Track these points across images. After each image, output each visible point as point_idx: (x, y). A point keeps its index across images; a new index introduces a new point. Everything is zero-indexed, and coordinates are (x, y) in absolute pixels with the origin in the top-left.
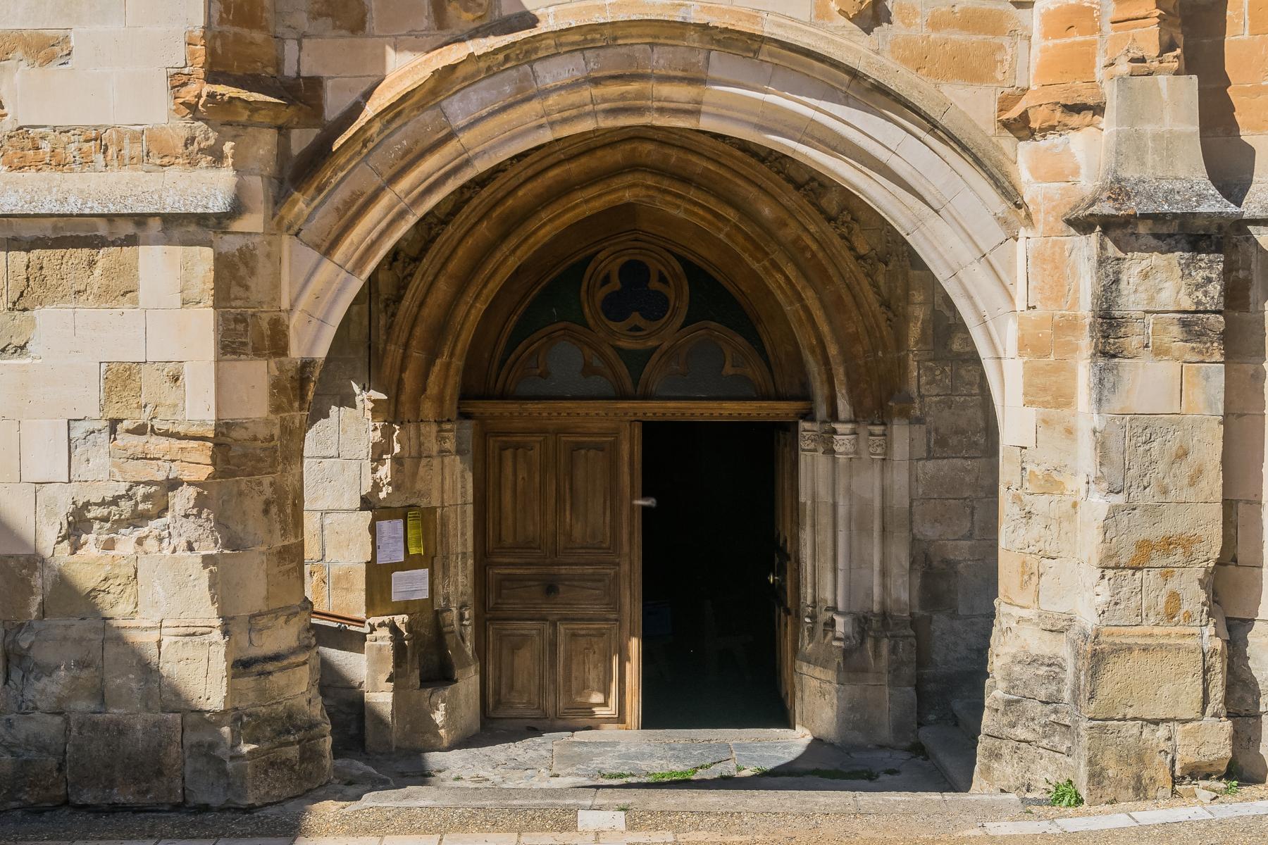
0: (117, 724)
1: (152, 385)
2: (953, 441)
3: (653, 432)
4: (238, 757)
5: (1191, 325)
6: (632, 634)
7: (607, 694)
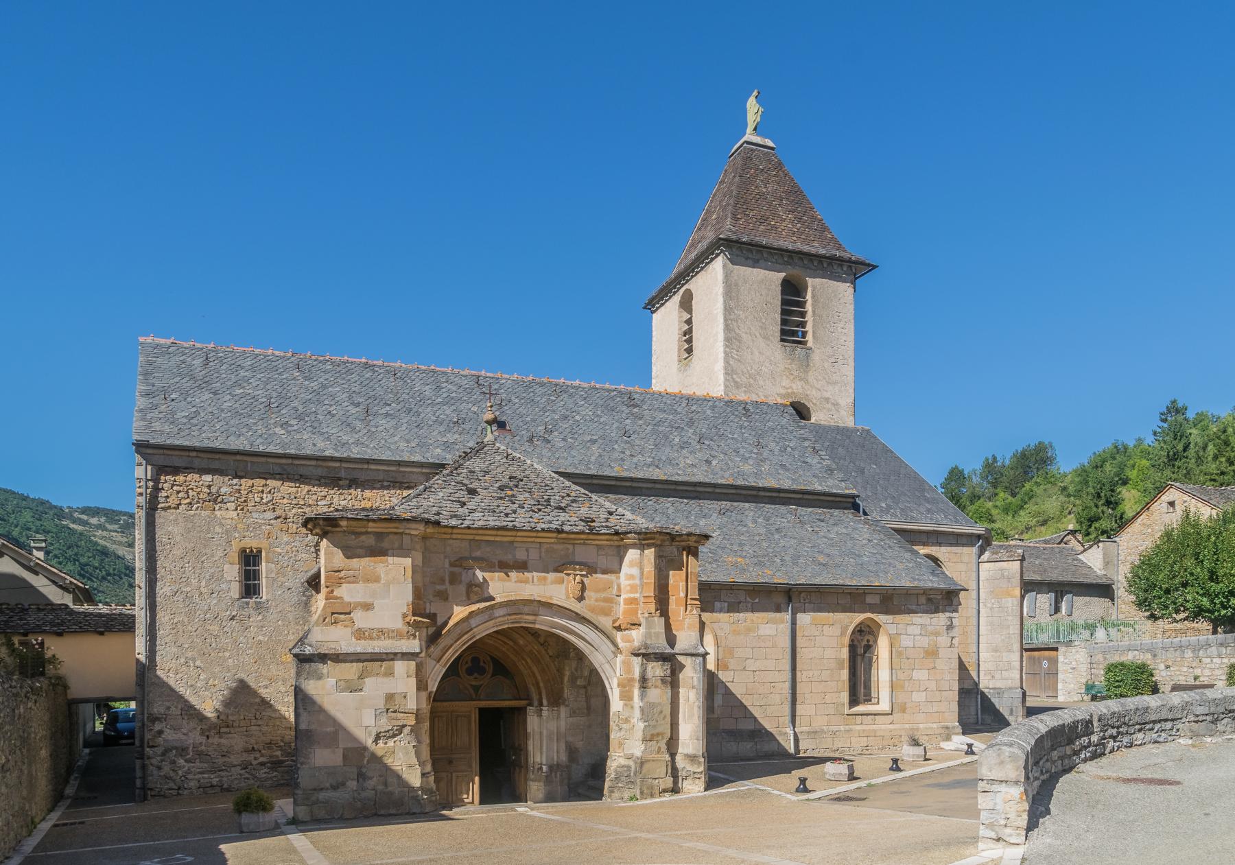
1: (398, 699)
2: (577, 711)
3: (482, 711)
4: (424, 799)
5: (663, 681)
7: (468, 795)
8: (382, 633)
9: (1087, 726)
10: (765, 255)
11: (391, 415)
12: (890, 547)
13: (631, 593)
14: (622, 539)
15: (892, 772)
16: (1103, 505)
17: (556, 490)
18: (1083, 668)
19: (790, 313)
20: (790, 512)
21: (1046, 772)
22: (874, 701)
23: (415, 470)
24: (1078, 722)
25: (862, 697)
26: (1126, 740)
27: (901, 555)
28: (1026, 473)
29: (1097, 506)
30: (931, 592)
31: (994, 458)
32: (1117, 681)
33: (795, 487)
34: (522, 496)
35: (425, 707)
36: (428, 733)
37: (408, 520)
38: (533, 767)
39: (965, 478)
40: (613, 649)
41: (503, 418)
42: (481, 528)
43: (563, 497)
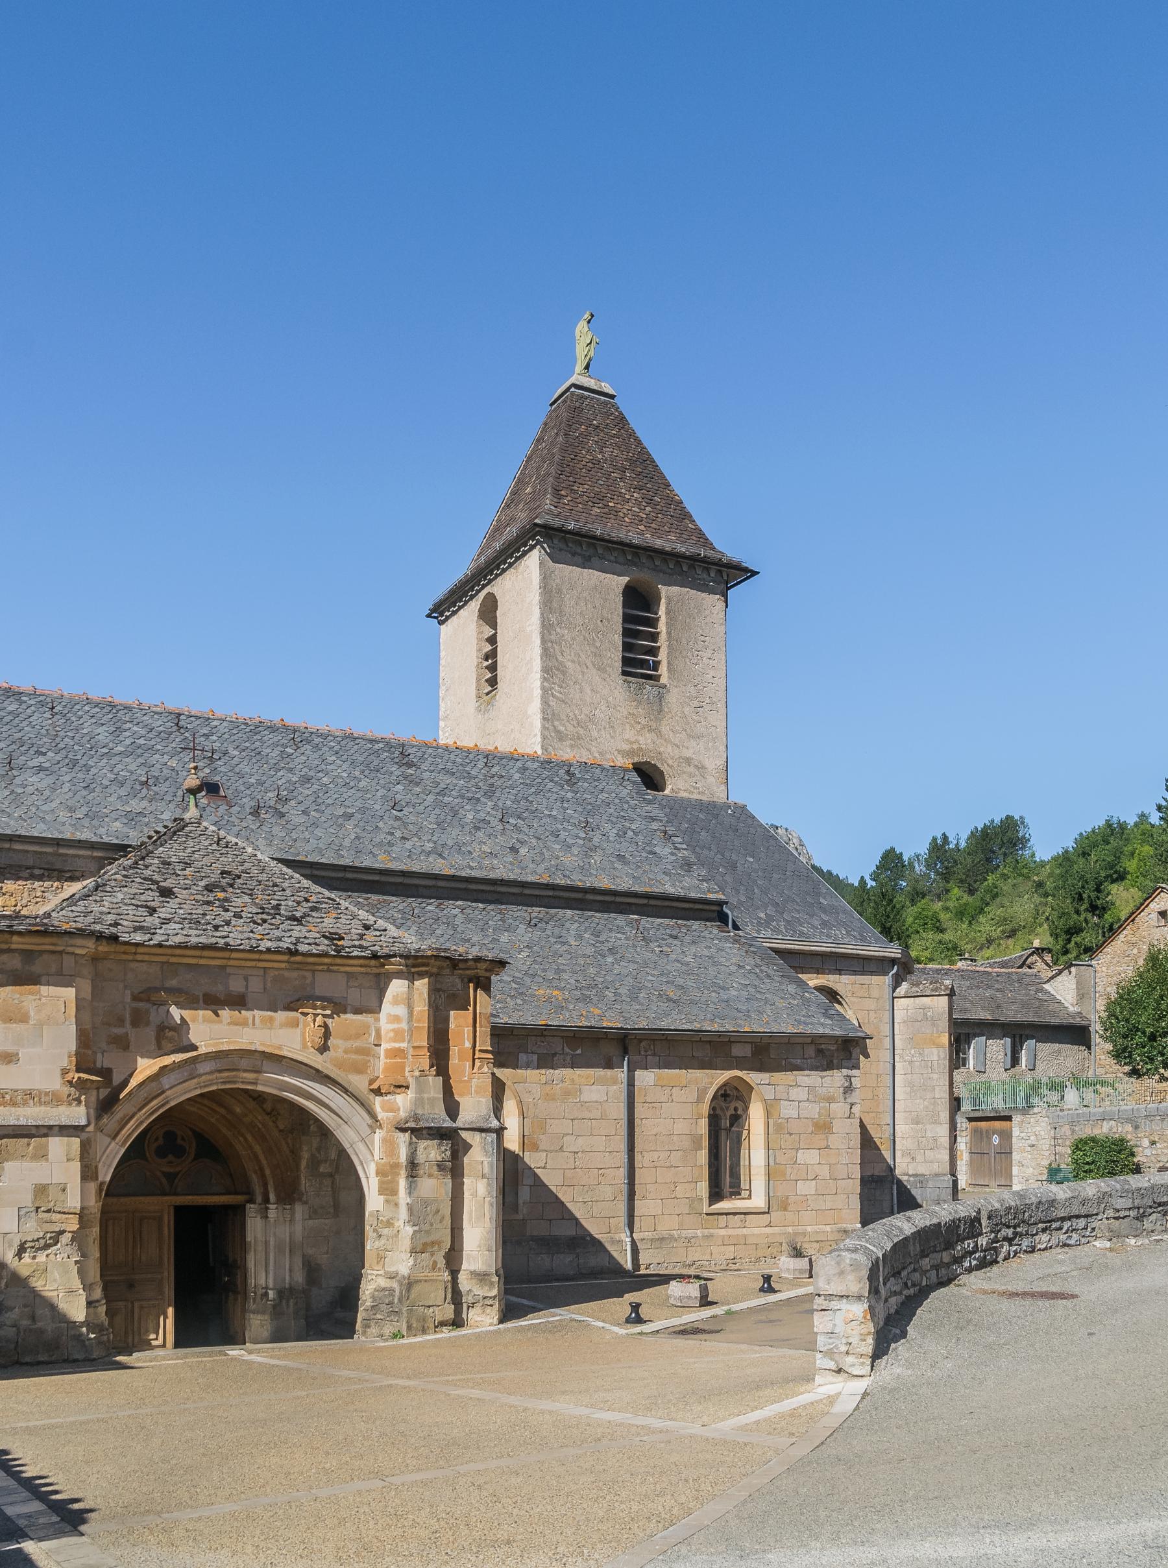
0: (40, 1329)
1: (53, 1193)
3: (179, 1210)
4: (91, 1339)
5: (440, 1167)
6: (169, 1306)
7: (157, 1335)
8: (30, 1096)
9: (972, 1225)
10: (600, 551)
11: (46, 769)
12: (768, 976)
13: (395, 1041)
14: (383, 965)
15: (762, 1293)
16: (1086, 910)
17: (288, 893)
18: (1045, 1145)
19: (637, 634)
20: (630, 924)
21: (914, 1285)
22: (744, 1194)
23: (81, 852)
24: (959, 1220)
25: (727, 1189)
26: (1026, 1243)
27: (783, 988)
28: (988, 860)
29: (1078, 912)
30: (822, 1041)
31: (945, 838)
32: (1088, 1163)
33: (637, 888)
34: (239, 900)
35: (95, 1206)
36: (97, 1242)
37: (70, 933)
38: (255, 1293)
39: (904, 866)
40: (369, 1121)
41: (216, 779)
42: (179, 946)
43: (298, 903)
